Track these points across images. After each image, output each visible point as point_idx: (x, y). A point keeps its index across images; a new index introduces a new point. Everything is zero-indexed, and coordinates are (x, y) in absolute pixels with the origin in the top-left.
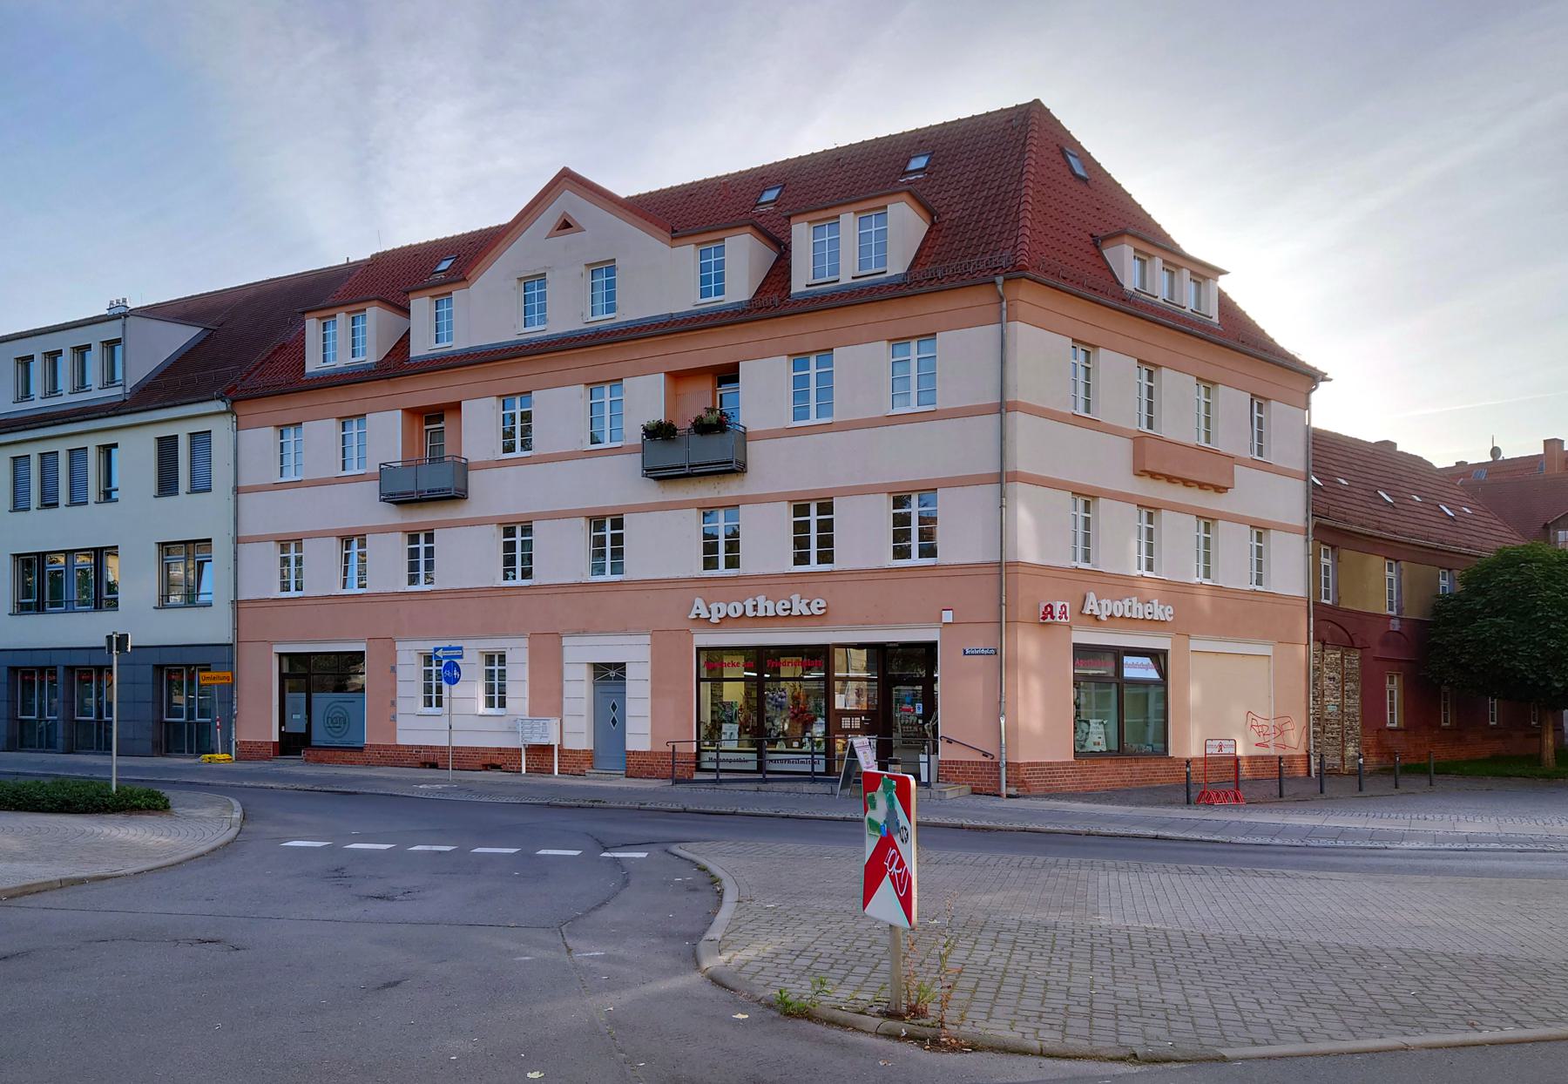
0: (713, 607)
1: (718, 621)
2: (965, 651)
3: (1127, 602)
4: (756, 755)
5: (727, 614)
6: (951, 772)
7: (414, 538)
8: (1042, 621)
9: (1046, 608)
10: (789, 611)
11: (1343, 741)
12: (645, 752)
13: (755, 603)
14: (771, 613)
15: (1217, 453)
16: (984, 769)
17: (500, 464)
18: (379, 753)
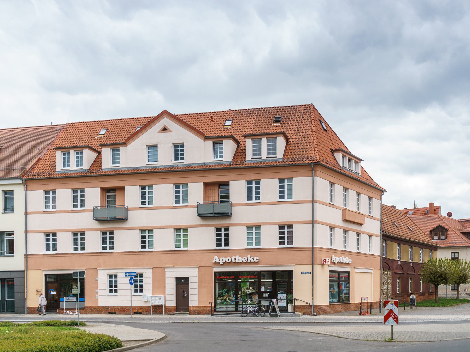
0: (221, 259)
1: (223, 263)
2: (301, 273)
3: (341, 258)
4: (235, 306)
5: (226, 261)
6: (297, 309)
7: (104, 233)
8: (322, 264)
9: (324, 260)
10: (246, 261)
11: (388, 297)
12: (196, 306)
13: (235, 258)
14: (241, 261)
15: (360, 214)
16: (307, 308)
17: (141, 209)
18: (91, 310)
